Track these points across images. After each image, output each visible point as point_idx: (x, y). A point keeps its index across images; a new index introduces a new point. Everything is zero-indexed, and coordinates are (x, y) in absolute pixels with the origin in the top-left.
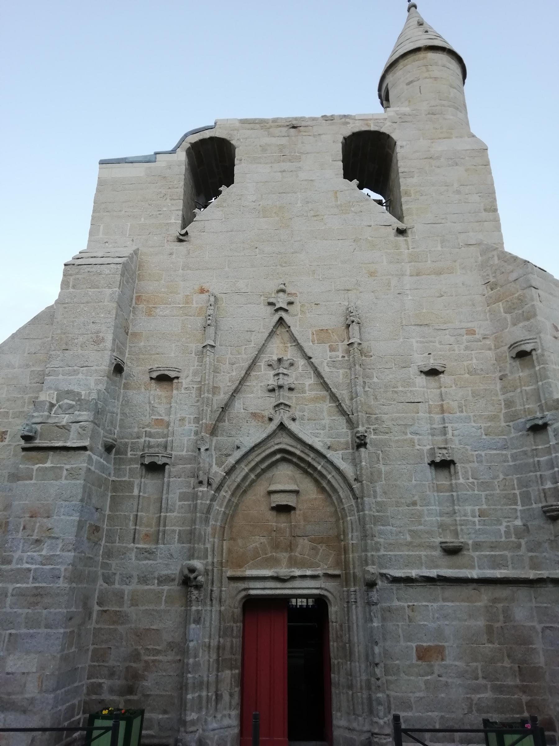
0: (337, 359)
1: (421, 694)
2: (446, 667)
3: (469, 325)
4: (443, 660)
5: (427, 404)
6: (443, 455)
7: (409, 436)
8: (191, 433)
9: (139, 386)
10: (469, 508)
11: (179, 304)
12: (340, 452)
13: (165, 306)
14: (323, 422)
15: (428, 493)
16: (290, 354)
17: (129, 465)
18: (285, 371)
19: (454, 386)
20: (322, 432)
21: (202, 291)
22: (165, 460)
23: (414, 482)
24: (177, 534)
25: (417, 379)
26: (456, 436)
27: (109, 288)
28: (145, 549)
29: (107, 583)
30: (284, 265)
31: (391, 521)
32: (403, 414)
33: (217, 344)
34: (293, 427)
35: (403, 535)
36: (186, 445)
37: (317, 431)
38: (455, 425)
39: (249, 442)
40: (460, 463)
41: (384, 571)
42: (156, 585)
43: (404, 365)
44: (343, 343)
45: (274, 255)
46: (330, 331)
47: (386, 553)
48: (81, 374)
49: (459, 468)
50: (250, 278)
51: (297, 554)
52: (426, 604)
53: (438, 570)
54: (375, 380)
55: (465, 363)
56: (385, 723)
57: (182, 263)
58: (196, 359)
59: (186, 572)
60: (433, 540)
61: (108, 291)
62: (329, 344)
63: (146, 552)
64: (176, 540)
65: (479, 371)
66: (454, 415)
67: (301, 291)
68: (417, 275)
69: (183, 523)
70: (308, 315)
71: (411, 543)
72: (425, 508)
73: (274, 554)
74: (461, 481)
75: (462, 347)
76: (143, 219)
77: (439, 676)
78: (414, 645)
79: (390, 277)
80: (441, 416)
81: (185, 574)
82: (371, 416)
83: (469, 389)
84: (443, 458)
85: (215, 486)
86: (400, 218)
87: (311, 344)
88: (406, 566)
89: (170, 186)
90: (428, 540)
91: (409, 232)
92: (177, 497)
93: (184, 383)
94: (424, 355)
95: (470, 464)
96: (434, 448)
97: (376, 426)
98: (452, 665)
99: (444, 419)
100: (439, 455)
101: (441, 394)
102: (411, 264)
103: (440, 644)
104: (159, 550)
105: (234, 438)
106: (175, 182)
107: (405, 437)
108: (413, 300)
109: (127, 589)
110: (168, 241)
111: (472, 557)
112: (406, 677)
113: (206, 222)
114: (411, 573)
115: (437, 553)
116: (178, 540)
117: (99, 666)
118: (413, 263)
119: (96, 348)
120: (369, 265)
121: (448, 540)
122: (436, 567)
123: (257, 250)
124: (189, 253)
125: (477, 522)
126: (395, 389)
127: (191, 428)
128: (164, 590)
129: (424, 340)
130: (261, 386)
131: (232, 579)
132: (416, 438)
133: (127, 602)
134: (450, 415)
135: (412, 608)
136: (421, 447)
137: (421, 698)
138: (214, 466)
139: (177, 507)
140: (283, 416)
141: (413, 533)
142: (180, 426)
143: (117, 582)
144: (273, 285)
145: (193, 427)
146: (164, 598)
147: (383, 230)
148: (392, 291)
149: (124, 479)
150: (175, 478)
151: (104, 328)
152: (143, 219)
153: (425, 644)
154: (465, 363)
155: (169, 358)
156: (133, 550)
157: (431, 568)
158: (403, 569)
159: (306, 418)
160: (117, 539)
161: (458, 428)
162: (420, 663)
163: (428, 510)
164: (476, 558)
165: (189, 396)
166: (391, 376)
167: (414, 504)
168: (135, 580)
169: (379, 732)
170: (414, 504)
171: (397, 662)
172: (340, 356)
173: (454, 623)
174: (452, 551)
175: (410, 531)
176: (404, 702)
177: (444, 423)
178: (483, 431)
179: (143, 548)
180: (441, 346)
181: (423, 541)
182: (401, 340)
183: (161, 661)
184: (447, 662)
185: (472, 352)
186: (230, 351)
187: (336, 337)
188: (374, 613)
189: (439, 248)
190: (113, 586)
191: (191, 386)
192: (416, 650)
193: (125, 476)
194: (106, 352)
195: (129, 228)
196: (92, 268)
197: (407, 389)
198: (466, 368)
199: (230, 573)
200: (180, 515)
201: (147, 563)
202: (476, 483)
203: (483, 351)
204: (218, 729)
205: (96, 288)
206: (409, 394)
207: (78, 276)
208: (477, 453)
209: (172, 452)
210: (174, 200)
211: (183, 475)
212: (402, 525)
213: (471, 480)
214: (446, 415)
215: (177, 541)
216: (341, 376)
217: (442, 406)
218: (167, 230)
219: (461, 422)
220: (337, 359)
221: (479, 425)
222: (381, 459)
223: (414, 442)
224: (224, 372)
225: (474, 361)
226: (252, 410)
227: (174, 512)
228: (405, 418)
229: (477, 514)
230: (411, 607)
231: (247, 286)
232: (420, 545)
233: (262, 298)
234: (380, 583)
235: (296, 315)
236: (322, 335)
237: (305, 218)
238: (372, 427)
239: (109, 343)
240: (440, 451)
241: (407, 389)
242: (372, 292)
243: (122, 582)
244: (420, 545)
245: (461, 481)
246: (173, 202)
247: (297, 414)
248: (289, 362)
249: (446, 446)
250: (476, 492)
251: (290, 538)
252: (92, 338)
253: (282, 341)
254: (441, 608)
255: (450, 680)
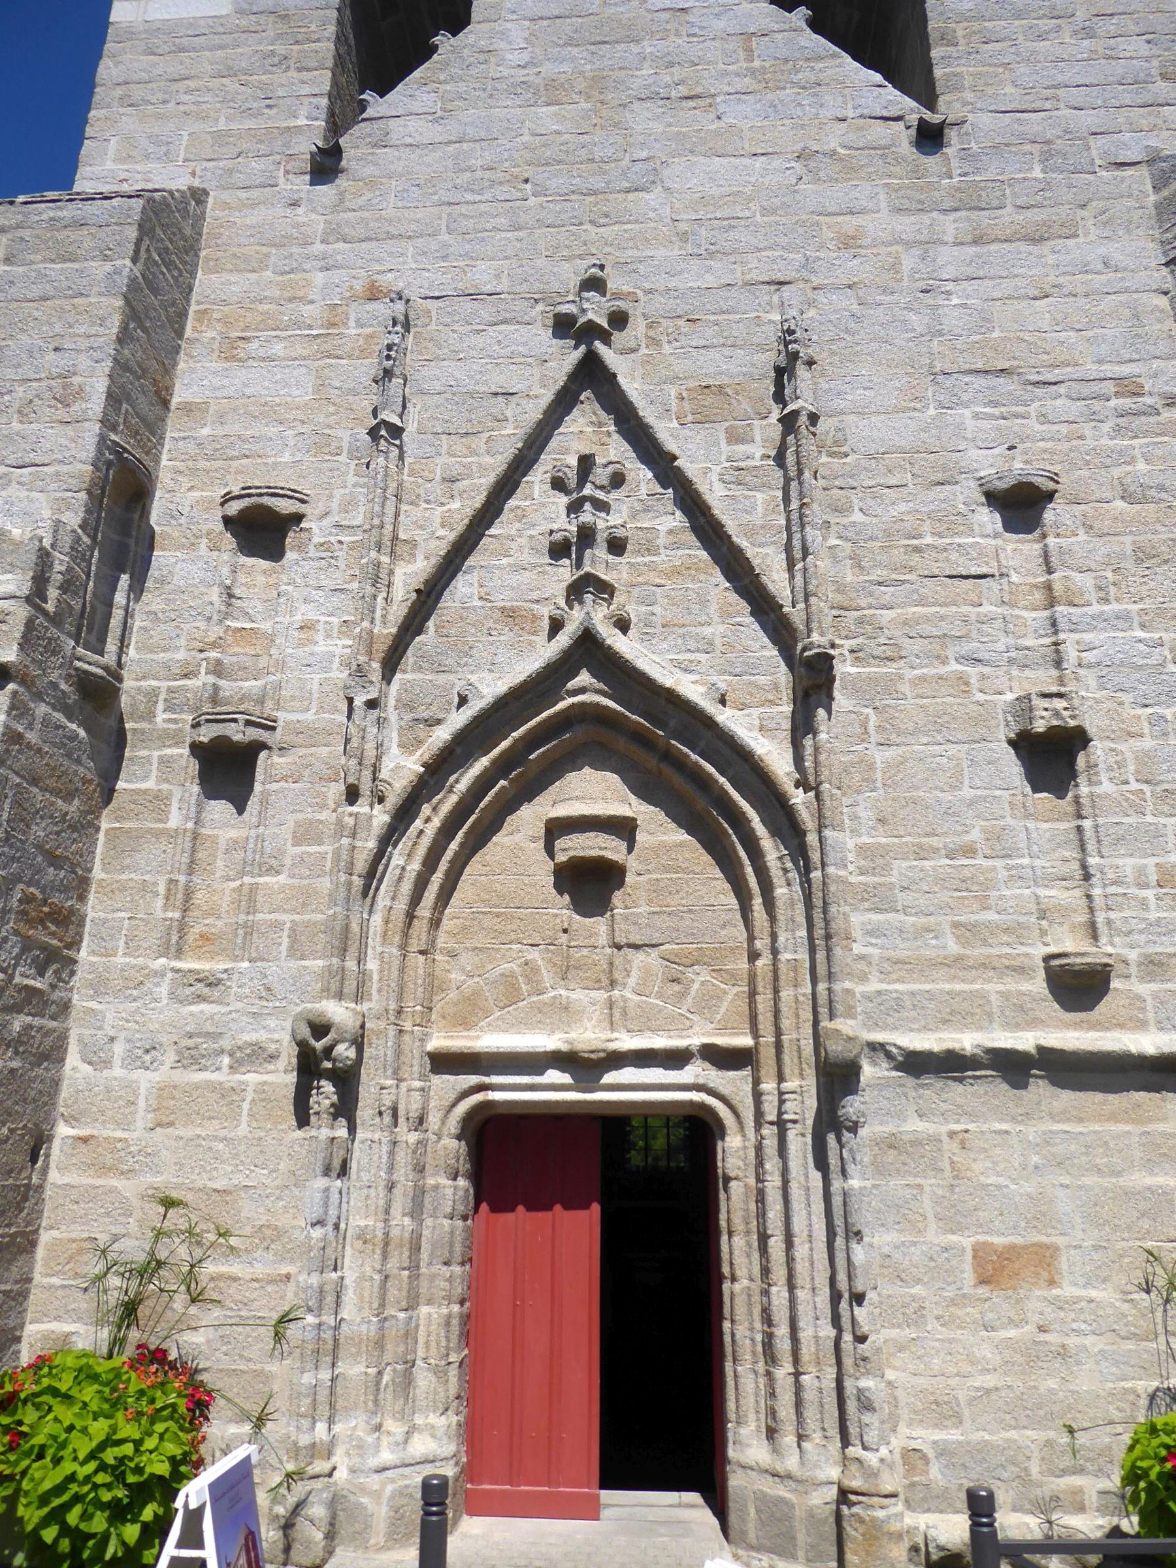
0: (749, 463)
1: (989, 1381)
2: (1059, 1304)
3: (1125, 370)
4: (1052, 1283)
5: (1004, 580)
6: (1057, 714)
7: (954, 666)
8: (332, 662)
9: (193, 540)
10: (1128, 865)
11: (310, 327)
12: (755, 712)
13: (274, 333)
14: (707, 631)
15: (1009, 821)
16: (616, 450)
17: (160, 748)
18: (600, 495)
19: (1081, 531)
20: (703, 657)
21: (373, 294)
22: (254, 734)
23: (967, 793)
24: (286, 933)
25: (976, 516)
26: (1090, 666)
27: (106, 258)
28: (197, 972)
29: (90, 1063)
30: (602, 221)
31: (903, 899)
32: (938, 609)
33: (411, 428)
34: (623, 645)
35: (936, 937)
36: (316, 695)
37: (688, 656)
38: (1088, 637)
39: (491, 687)
40: (1101, 739)
41: (879, 1037)
42: (226, 1070)
43: (939, 477)
44: (764, 422)
45: (573, 197)
46: (729, 391)
47: (884, 986)
48: (14, 485)
49: (1099, 752)
50: (506, 258)
51: (628, 994)
52: (1005, 1126)
53: (1039, 1034)
54: (858, 517)
55: (1116, 472)
56: (882, 1460)
57: (322, 226)
58: (353, 467)
59: (305, 1032)
60: (1023, 950)
61: (99, 269)
62: (727, 424)
63: (199, 980)
64: (284, 948)
65: (1153, 492)
66: (1085, 609)
67: (648, 286)
68: (975, 242)
69: (304, 905)
70: (667, 349)
71: (959, 958)
72: (1000, 863)
73: (563, 992)
74: (1106, 787)
75: (1106, 427)
76: (222, 120)
77: (1042, 1329)
78: (967, 1242)
79: (900, 248)
80: (1047, 613)
81: (299, 1037)
82: (846, 613)
83: (1128, 539)
84: (1055, 723)
85: (392, 801)
86: (928, 98)
87: (675, 424)
88: (945, 1022)
89: (299, 37)
90: (1009, 951)
91: (951, 134)
92: (286, 833)
93: (316, 530)
94: (996, 451)
95: (1132, 741)
96: (1028, 697)
97: (860, 640)
98: (1080, 1299)
99: (1054, 624)
100: (1044, 713)
101: (1046, 555)
102: (957, 214)
103: (1044, 1239)
104: (235, 977)
105: (451, 677)
106: (313, 27)
107: (943, 670)
108: (964, 306)
109: (145, 1080)
110: (287, 172)
111: (1139, 997)
112: (944, 1333)
113: (392, 122)
114: (959, 1041)
115: (1038, 985)
116: (291, 948)
117: (64, 1287)
118: (963, 213)
119: (61, 414)
120: (840, 219)
121: (1069, 950)
122: (1034, 1023)
123: (528, 186)
124: (342, 201)
125: (1152, 902)
126: (915, 542)
127: (331, 649)
128: (246, 1083)
129: (996, 411)
130: (531, 537)
131: (444, 1062)
132: (973, 671)
133: (142, 1118)
134: (1072, 610)
135: (961, 1139)
136: (988, 698)
137: (988, 1392)
138: (395, 750)
139: (288, 861)
140: (597, 615)
141: (967, 932)
142: (301, 644)
143: (117, 1061)
144: (570, 275)
145: (341, 646)
146: (246, 1106)
147: (881, 132)
148: (905, 283)
149: (143, 786)
150: (282, 783)
151: (84, 362)
152: (222, 120)
153: (998, 1240)
154: (1116, 472)
155: (279, 465)
156: (163, 975)
157: (1017, 1027)
158: (937, 1029)
159: (658, 621)
160: (122, 943)
161: (1097, 643)
162: (983, 1291)
163: (1008, 868)
164: (1149, 1001)
165: (330, 566)
166: (903, 507)
167: (969, 851)
168: (170, 1057)
169: (864, 1489)
170: (969, 851)
171: (917, 1290)
172: (758, 455)
173: (1086, 1181)
174: (1079, 987)
175: (956, 925)
176: (937, 1404)
177: (1056, 633)
178: (1167, 653)
179: (190, 971)
180: (1044, 427)
181: (995, 951)
182: (932, 411)
183: (236, 1279)
184: (1067, 1290)
185: (1135, 441)
186: (445, 447)
187: (746, 405)
188: (851, 1150)
189: (1037, 173)
190: (106, 1073)
191: (333, 539)
192: (974, 1257)
193: (146, 778)
194: (87, 424)
195: (184, 143)
196: (60, 208)
197: (948, 541)
198: (1116, 482)
199: (436, 1043)
200: (296, 881)
201: (202, 1012)
202: (1148, 794)
203: (1166, 439)
204: (396, 1467)
205: (70, 260)
206: (954, 556)
207: (20, 233)
208: (1150, 710)
209: (280, 715)
210: (308, 70)
211: (306, 773)
212: (932, 909)
213: (1134, 786)
214: (1061, 609)
215: (284, 953)
216: (760, 509)
217: (1049, 587)
218: (287, 145)
219: (1104, 629)
220: (749, 463)
221: (1157, 636)
222: (871, 729)
223: (967, 684)
224: (427, 502)
225: (1141, 466)
226: (501, 599)
227: (278, 873)
228: (942, 618)
229: (1153, 878)
230: (961, 1136)
231: (498, 276)
232: (985, 965)
233: (540, 307)
234: (868, 1072)
235: (633, 351)
236: (707, 402)
237: (661, 103)
238: (848, 644)
239: (96, 403)
240: (1046, 703)
241: (948, 541)
242: (849, 287)
243: (133, 1061)
244: (985, 965)
245: (1106, 787)
246: (306, 75)
247: (634, 611)
248: (610, 469)
249: (1063, 690)
250: (1149, 819)
251: (609, 951)
252: (50, 389)
253: (594, 419)
254: (1048, 1139)
255: (1072, 1341)
